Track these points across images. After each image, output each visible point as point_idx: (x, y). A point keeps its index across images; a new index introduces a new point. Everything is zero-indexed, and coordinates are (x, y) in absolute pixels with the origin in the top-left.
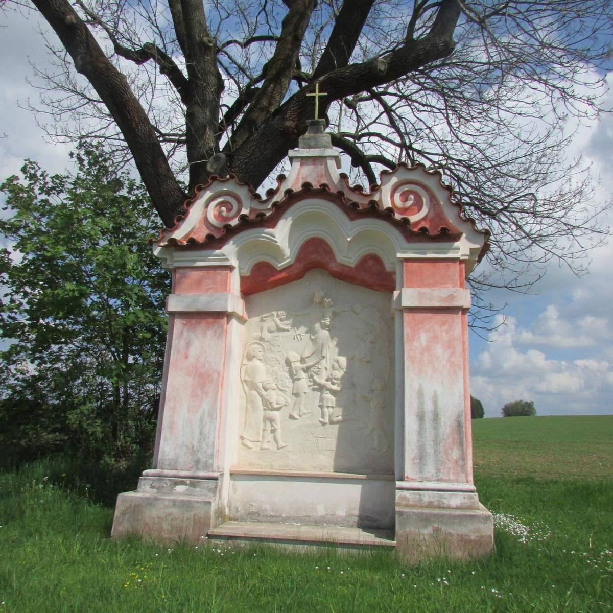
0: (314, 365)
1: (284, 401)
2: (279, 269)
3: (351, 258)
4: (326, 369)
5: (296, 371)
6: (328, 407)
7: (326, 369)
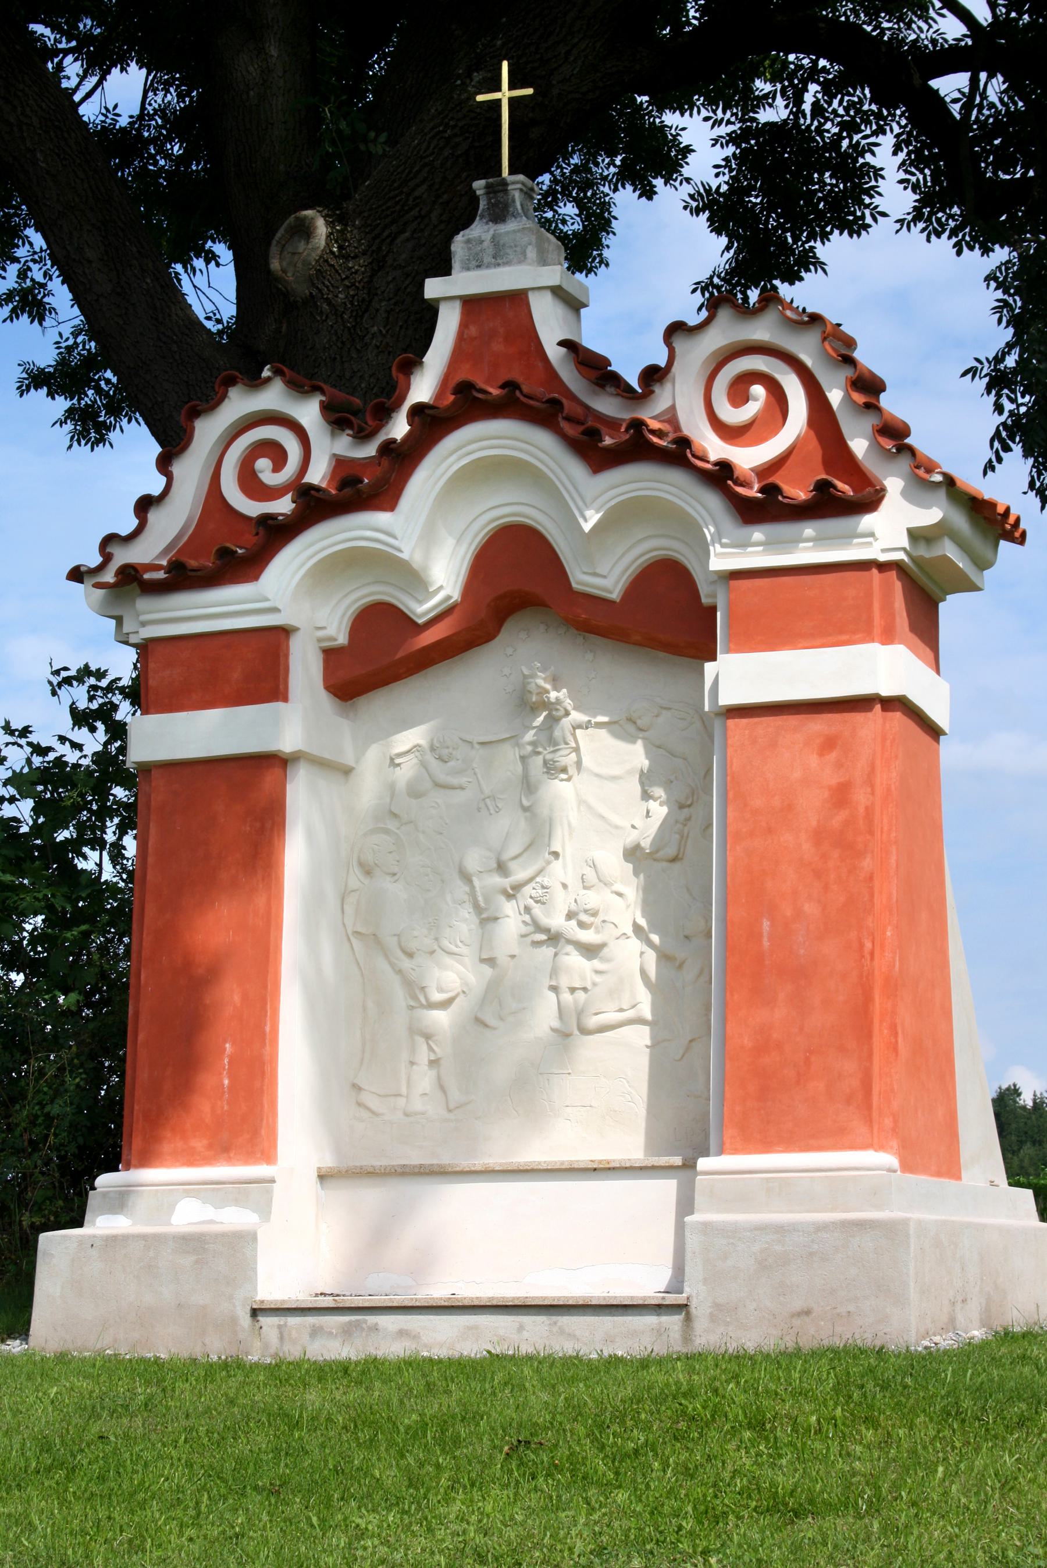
0: (531, 880)
1: (458, 980)
2: (420, 621)
3: (604, 577)
4: (565, 886)
5: (487, 900)
6: (573, 990)
7: (565, 886)
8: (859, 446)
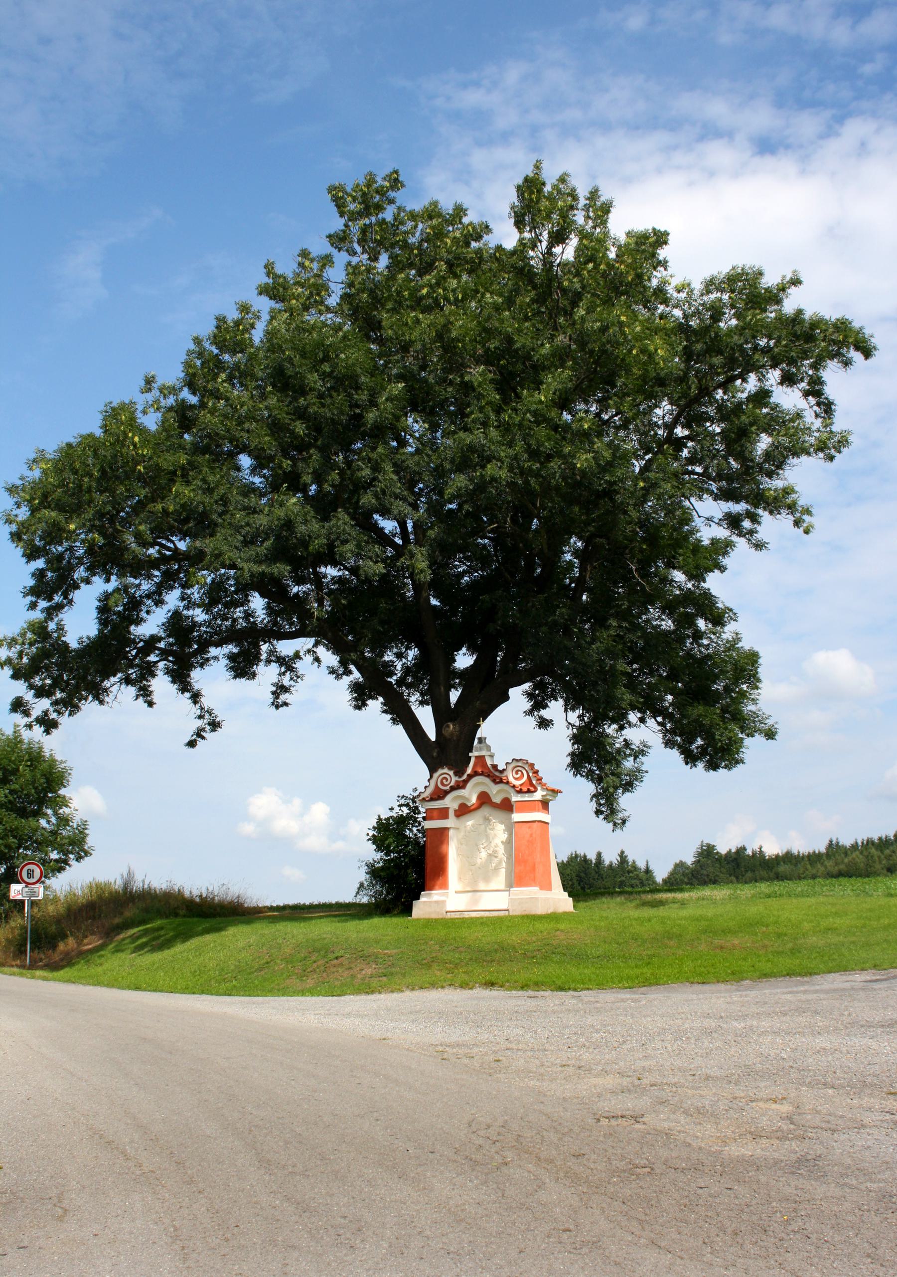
8: (534, 782)
